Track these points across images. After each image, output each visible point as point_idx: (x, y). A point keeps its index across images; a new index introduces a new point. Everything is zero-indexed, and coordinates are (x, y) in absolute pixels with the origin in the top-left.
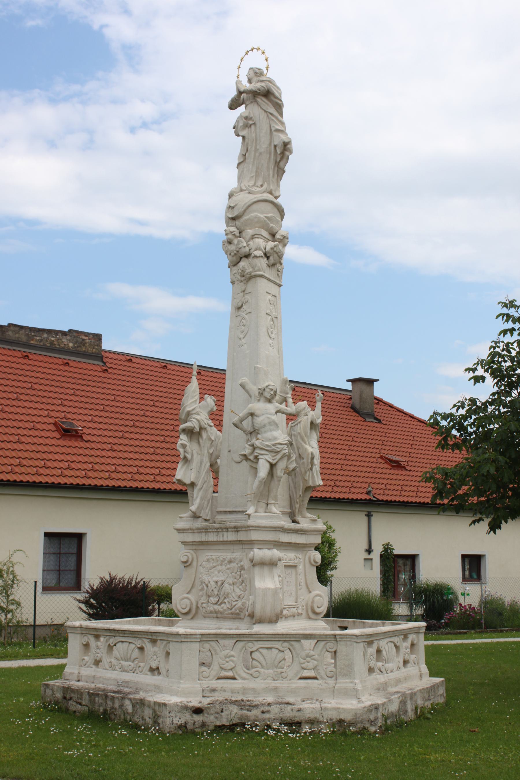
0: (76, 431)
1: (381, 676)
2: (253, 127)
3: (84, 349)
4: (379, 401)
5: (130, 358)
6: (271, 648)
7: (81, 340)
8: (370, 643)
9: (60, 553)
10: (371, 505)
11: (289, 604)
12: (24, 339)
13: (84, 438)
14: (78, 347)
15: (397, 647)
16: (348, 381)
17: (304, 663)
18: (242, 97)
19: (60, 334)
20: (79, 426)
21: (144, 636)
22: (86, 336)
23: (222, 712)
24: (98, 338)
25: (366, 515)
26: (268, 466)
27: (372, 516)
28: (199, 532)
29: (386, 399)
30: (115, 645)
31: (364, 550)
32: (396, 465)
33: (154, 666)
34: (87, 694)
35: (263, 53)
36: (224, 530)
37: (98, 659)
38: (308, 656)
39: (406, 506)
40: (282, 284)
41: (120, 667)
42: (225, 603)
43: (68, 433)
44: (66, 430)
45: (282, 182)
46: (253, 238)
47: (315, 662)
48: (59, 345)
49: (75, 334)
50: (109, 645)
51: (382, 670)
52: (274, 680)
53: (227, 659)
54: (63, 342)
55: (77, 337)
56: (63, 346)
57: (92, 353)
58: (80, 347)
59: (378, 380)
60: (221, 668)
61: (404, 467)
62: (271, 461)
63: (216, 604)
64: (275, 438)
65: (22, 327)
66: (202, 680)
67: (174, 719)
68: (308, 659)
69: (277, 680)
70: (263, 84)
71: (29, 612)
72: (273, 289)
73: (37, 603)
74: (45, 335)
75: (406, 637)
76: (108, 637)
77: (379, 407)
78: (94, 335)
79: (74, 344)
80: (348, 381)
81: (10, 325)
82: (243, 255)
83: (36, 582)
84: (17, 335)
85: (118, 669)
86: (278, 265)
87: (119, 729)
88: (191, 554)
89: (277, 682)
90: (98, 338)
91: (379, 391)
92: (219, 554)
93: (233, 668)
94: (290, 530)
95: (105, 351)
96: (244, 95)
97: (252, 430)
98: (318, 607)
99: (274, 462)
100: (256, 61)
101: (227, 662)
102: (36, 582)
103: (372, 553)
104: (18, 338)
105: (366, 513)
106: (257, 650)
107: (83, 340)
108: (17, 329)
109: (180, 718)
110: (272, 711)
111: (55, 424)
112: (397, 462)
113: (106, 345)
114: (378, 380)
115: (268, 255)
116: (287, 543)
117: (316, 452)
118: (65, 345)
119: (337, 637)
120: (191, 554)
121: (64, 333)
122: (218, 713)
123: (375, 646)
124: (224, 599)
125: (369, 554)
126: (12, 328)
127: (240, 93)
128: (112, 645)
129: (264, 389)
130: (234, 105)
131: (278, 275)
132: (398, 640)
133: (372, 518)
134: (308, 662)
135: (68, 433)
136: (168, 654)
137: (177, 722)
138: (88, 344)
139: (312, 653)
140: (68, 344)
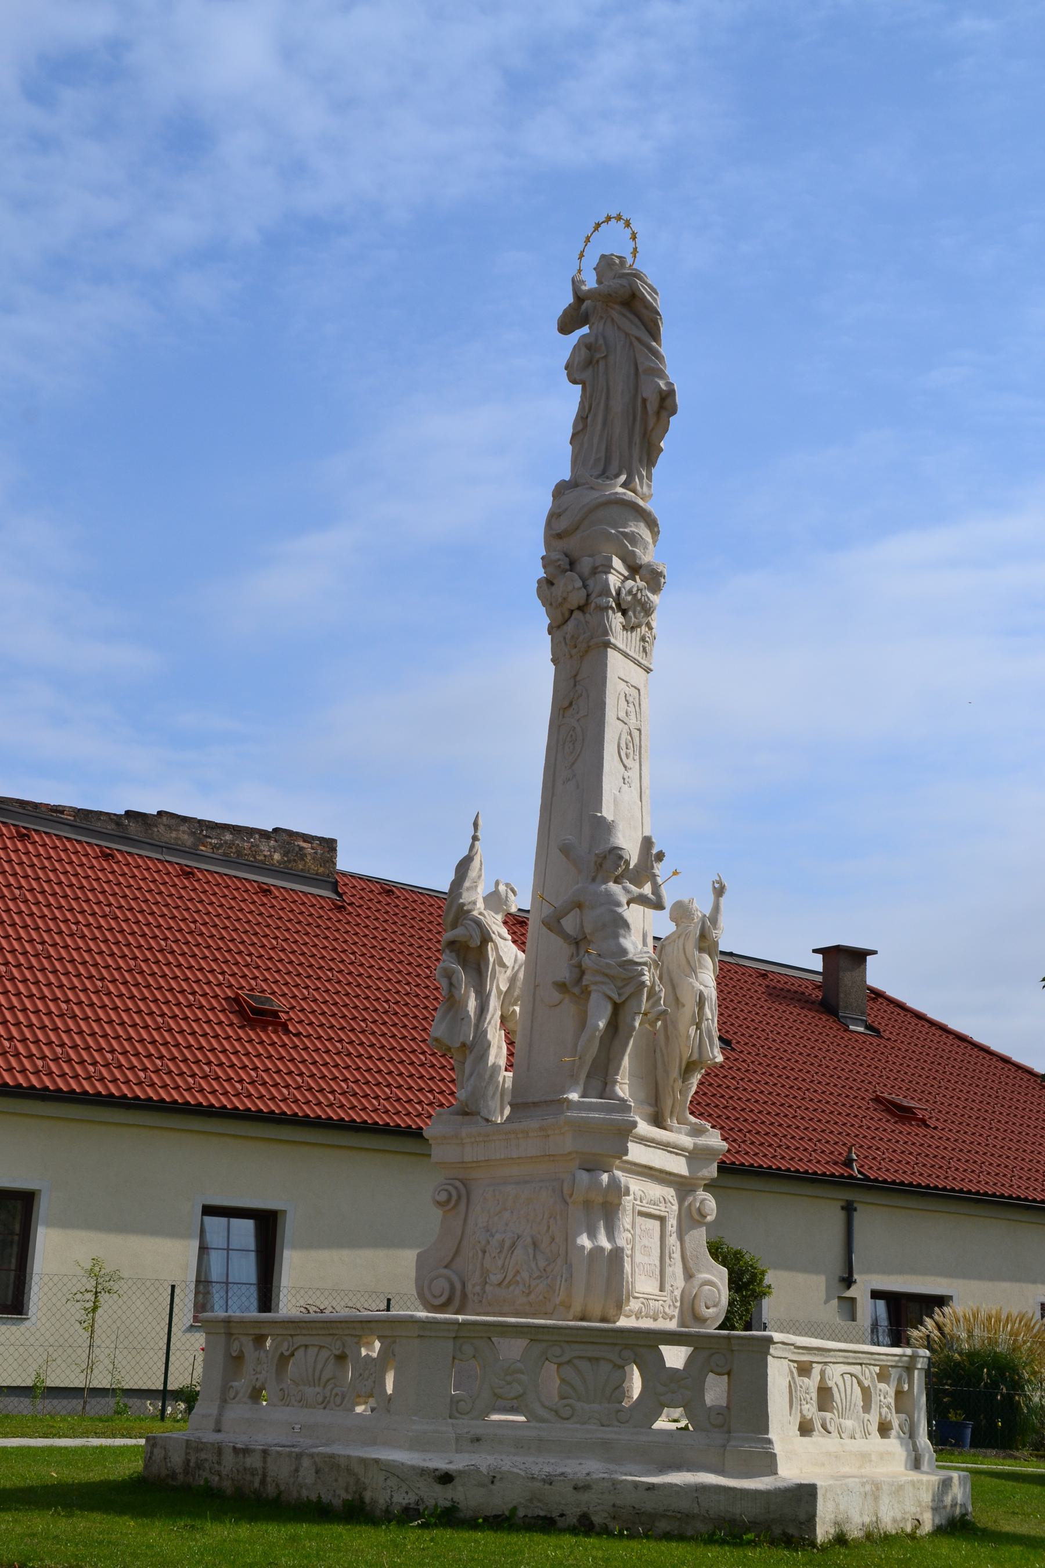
0: (275, 1014)
1: (829, 1440)
2: (602, 363)
3: (301, 867)
4: (877, 995)
5: (388, 889)
6: (597, 1359)
7: (297, 849)
10: (851, 1187)
11: (646, 1291)
12: (188, 840)
13: (291, 1028)
14: (289, 861)
15: (866, 1392)
16: (815, 951)
18: (584, 307)
19: (257, 836)
20: (280, 1004)
21: (347, 1332)
22: (305, 841)
23: (493, 1482)
24: (329, 845)
25: (843, 1208)
26: (609, 1009)
27: (855, 1210)
29: (890, 993)
30: (292, 1355)
31: (837, 1278)
32: (903, 1114)
34: (231, 1450)
35: (628, 224)
36: (520, 1136)
37: (258, 1385)
39: (924, 1194)
40: (651, 667)
41: (298, 1399)
42: (518, 1283)
43: (257, 1016)
44: (256, 1011)
45: (653, 471)
46: (595, 573)
48: (255, 858)
49: (285, 837)
51: (830, 1429)
52: (603, 1426)
53: (508, 1378)
54: (262, 851)
55: (289, 843)
56: (261, 858)
57: (317, 874)
58: (294, 860)
59: (874, 952)
60: (495, 1394)
61: (923, 1122)
62: (615, 996)
63: (500, 1284)
65: (185, 819)
66: (456, 1418)
67: (395, 1495)
69: (608, 1426)
70: (623, 282)
71: (156, 1347)
72: (636, 675)
74: (228, 837)
76: (280, 1338)
77: (876, 1006)
78: (322, 840)
79: (285, 854)
80: (815, 951)
81: (160, 813)
82: (576, 606)
83: (173, 1287)
84: (174, 835)
85: (296, 1404)
86: (644, 628)
88: (456, 1188)
89: (607, 1429)
90: (329, 845)
91: (877, 975)
93: (520, 1396)
94: (652, 1141)
95: (344, 874)
96: (587, 303)
97: (580, 937)
99: (618, 1001)
100: (613, 242)
101: (509, 1383)
102: (173, 1287)
103: (853, 1288)
104: (176, 838)
105: (843, 1204)
106: (568, 1362)
107: (301, 849)
108: (173, 822)
109: (407, 1493)
110: (595, 1487)
111: (237, 1000)
112: (909, 1110)
113: (345, 862)
114: (874, 952)
115: (624, 607)
116: (645, 1167)
117: (711, 992)
118: (265, 856)
119: (733, 1342)
120: (456, 1188)
121: (264, 834)
122: (483, 1486)
124: (515, 1276)
125: (849, 1287)
126: (165, 819)
127: (579, 298)
128: (287, 1354)
129: (605, 857)
130: (566, 325)
131: (644, 649)
133: (856, 1215)
135: (257, 1016)
137: (401, 1500)
138: (309, 857)
140: (271, 856)
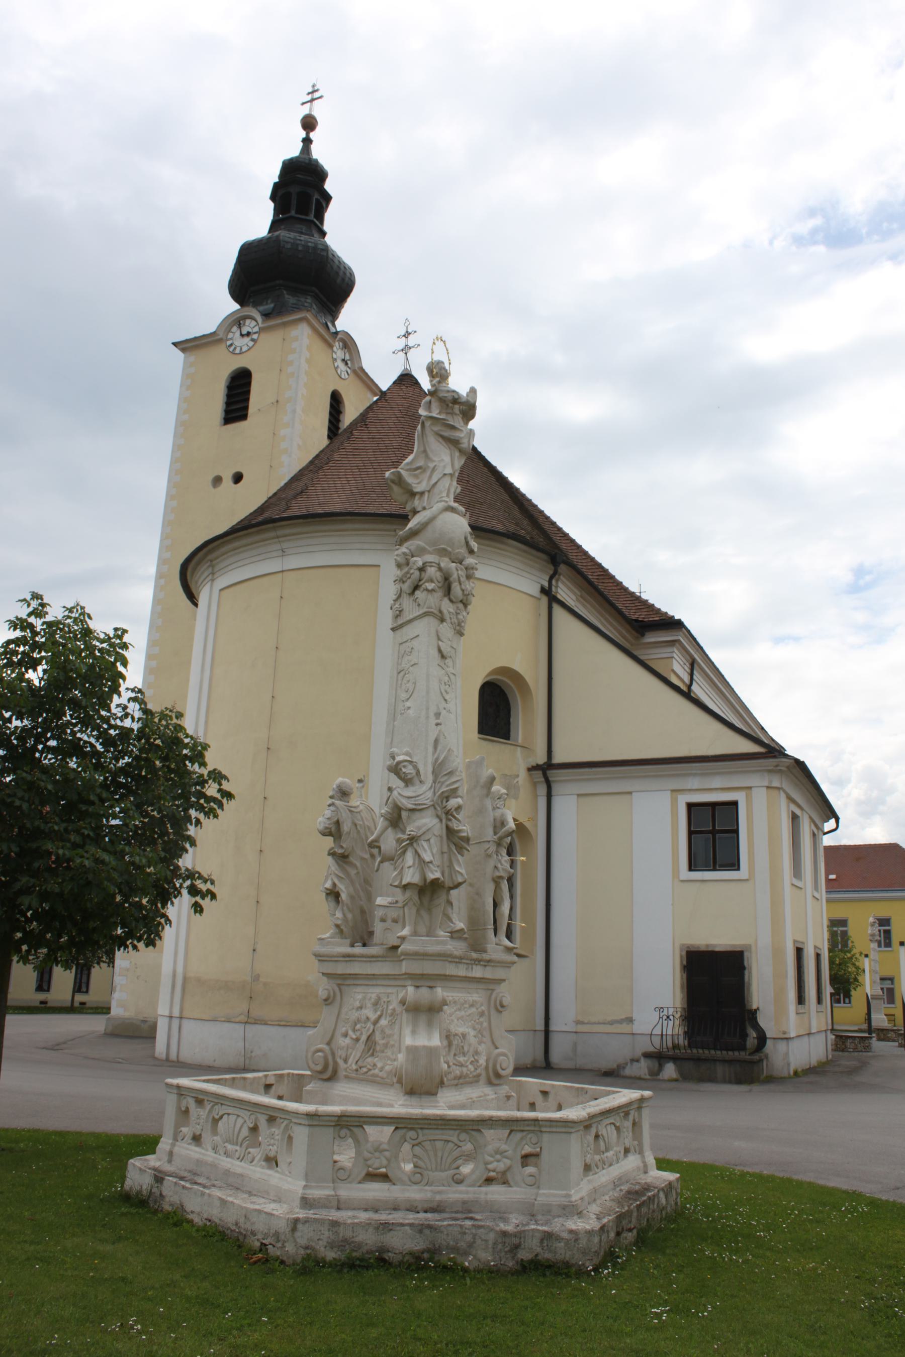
8: (587, 1127)
9: (181, 1018)
15: (618, 1129)
17: (491, 1163)
28: (346, 961)
33: (272, 1154)
38: (498, 1152)
47: (508, 1162)
50: (213, 1117)
64: (425, 825)
68: (498, 1157)
73: (238, 587)
75: (627, 1114)
87: (83, 779)
92: (460, 995)
98: (503, 1070)
123: (593, 1131)
128: (217, 1117)
132: (616, 1119)
134: (498, 1161)
136: (290, 1138)
139: (504, 1147)
